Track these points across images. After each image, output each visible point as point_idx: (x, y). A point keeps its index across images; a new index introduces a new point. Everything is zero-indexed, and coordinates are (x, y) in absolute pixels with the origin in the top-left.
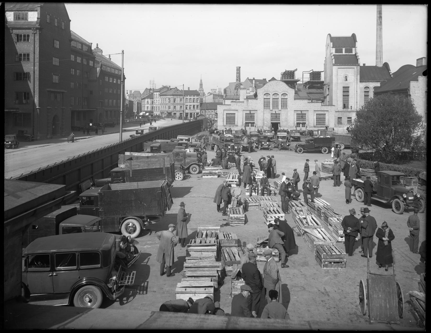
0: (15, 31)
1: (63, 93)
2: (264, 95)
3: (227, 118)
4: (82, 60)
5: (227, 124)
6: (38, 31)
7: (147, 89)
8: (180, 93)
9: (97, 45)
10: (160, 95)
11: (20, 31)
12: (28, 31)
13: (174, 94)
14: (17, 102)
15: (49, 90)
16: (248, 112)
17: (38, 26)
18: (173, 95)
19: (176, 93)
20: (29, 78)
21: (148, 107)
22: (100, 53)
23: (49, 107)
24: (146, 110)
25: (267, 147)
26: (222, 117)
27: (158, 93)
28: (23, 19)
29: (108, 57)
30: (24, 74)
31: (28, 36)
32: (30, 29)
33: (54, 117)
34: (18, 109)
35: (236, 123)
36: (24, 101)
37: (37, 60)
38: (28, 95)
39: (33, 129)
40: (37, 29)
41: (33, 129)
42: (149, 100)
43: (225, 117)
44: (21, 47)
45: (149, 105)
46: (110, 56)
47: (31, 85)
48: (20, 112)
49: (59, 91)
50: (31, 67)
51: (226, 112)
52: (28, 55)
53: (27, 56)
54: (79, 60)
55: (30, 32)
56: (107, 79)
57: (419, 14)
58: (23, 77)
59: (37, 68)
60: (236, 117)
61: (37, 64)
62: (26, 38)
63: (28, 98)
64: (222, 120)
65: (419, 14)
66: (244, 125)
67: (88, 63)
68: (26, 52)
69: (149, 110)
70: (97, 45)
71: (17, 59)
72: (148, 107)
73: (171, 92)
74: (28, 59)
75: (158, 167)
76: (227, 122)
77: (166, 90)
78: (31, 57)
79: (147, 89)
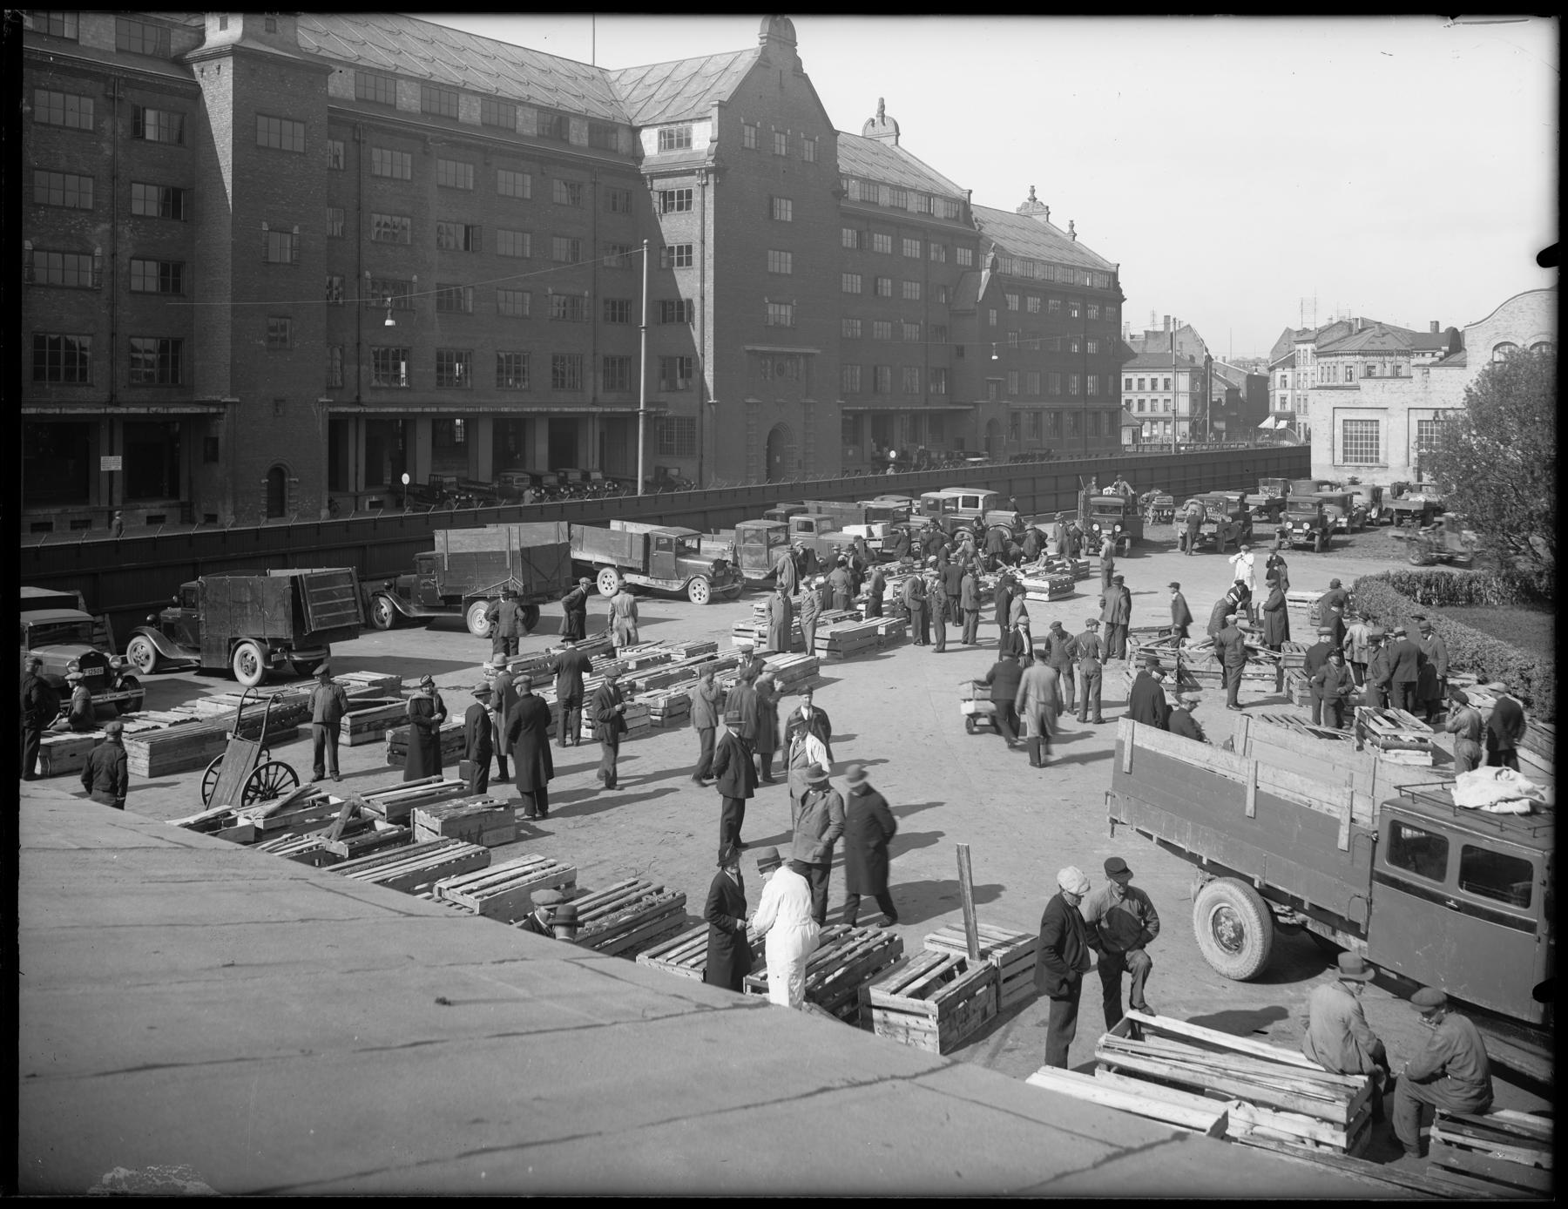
0: (659, 184)
1: (807, 355)
2: (1495, 348)
3: (1345, 437)
4: (925, 251)
5: (1345, 460)
6: (711, 176)
7: (1288, 332)
8: (1391, 344)
9: (1033, 191)
10: (1318, 354)
11: (670, 181)
12: (688, 179)
13: (1367, 347)
14: (663, 383)
15: (749, 348)
16: (1429, 416)
17: (710, 164)
18: (1364, 353)
19: (1378, 346)
20: (691, 314)
21: (1283, 399)
22: (1041, 219)
23: (750, 401)
24: (1278, 408)
25: (1302, 540)
26: (1329, 432)
27: (1310, 347)
28: (680, 145)
29: (1067, 230)
30: (681, 303)
31: (689, 193)
32: (691, 173)
33: (771, 433)
34: (665, 405)
35: (1381, 457)
36: (680, 383)
37: (710, 262)
38: (688, 365)
39: (701, 465)
40: (708, 171)
41: (701, 465)
42: (1288, 372)
43: (1339, 432)
44: (677, 228)
45: (1289, 392)
46: (1072, 226)
47: (696, 335)
48: (670, 413)
49: (779, 349)
50: (695, 284)
51: (1342, 415)
52: (689, 248)
53: (684, 254)
54: (912, 248)
55: (692, 182)
56: (1014, 302)
57: (1523, 53)
58: (674, 311)
59: (709, 286)
60: (1381, 435)
61: (710, 273)
62: (682, 201)
63: (689, 375)
64: (1328, 445)
65: (1523, 53)
66: (1414, 464)
67: (951, 257)
68: (683, 241)
69: (1289, 408)
70: (1033, 191)
71: (664, 265)
72: (1283, 399)
73: (1358, 342)
74: (689, 262)
75: (496, 549)
76: (1345, 452)
77: (1342, 334)
78: (696, 254)
79: (1288, 332)
